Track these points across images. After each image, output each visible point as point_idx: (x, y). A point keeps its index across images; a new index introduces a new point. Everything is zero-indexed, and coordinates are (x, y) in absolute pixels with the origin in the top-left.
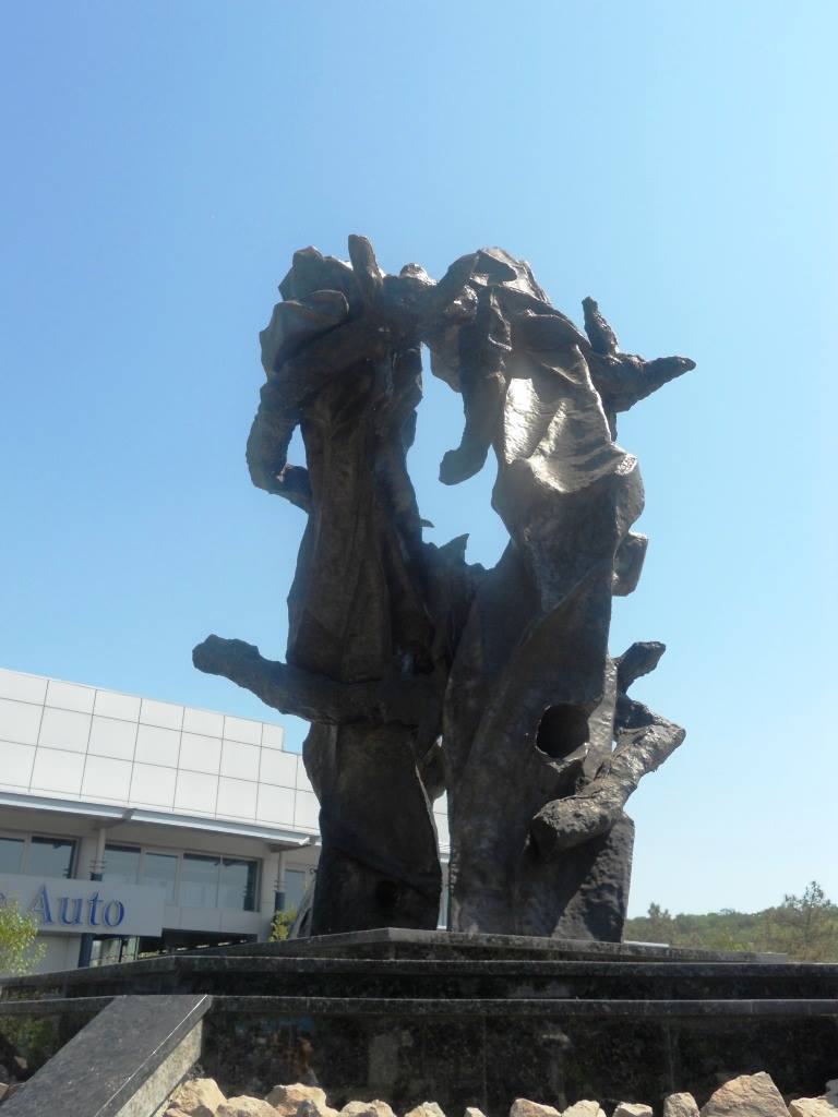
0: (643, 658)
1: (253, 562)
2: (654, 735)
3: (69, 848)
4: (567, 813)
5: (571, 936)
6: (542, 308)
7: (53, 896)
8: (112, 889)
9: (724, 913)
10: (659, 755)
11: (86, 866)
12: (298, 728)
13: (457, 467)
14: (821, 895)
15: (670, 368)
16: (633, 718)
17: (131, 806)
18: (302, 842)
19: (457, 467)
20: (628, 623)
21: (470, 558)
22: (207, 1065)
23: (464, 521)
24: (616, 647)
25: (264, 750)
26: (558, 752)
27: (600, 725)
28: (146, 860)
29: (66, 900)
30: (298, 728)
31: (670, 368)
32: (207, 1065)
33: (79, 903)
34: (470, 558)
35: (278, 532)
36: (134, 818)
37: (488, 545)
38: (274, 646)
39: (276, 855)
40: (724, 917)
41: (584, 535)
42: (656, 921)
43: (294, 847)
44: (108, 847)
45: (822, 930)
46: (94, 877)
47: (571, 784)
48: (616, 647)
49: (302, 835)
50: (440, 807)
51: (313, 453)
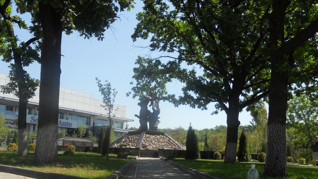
0: (159, 118)
4: (155, 126)
8: (70, 121)
9: (167, 129)
12: (139, 119)
16: (158, 121)
18: (99, 115)
19: (150, 106)
20: (159, 116)
23: (150, 109)
24: (158, 117)
28: (74, 117)
33: (65, 123)
35: (139, 108)
36: (75, 111)
37: (152, 111)
38: (139, 115)
39: (93, 117)
40: (167, 130)
41: (157, 112)
42: (159, 129)
43: (98, 116)
44: (69, 115)
45: (180, 133)
46: (67, 119)
47: (155, 125)
48: (158, 117)
50: (148, 124)
51: (74, 5)
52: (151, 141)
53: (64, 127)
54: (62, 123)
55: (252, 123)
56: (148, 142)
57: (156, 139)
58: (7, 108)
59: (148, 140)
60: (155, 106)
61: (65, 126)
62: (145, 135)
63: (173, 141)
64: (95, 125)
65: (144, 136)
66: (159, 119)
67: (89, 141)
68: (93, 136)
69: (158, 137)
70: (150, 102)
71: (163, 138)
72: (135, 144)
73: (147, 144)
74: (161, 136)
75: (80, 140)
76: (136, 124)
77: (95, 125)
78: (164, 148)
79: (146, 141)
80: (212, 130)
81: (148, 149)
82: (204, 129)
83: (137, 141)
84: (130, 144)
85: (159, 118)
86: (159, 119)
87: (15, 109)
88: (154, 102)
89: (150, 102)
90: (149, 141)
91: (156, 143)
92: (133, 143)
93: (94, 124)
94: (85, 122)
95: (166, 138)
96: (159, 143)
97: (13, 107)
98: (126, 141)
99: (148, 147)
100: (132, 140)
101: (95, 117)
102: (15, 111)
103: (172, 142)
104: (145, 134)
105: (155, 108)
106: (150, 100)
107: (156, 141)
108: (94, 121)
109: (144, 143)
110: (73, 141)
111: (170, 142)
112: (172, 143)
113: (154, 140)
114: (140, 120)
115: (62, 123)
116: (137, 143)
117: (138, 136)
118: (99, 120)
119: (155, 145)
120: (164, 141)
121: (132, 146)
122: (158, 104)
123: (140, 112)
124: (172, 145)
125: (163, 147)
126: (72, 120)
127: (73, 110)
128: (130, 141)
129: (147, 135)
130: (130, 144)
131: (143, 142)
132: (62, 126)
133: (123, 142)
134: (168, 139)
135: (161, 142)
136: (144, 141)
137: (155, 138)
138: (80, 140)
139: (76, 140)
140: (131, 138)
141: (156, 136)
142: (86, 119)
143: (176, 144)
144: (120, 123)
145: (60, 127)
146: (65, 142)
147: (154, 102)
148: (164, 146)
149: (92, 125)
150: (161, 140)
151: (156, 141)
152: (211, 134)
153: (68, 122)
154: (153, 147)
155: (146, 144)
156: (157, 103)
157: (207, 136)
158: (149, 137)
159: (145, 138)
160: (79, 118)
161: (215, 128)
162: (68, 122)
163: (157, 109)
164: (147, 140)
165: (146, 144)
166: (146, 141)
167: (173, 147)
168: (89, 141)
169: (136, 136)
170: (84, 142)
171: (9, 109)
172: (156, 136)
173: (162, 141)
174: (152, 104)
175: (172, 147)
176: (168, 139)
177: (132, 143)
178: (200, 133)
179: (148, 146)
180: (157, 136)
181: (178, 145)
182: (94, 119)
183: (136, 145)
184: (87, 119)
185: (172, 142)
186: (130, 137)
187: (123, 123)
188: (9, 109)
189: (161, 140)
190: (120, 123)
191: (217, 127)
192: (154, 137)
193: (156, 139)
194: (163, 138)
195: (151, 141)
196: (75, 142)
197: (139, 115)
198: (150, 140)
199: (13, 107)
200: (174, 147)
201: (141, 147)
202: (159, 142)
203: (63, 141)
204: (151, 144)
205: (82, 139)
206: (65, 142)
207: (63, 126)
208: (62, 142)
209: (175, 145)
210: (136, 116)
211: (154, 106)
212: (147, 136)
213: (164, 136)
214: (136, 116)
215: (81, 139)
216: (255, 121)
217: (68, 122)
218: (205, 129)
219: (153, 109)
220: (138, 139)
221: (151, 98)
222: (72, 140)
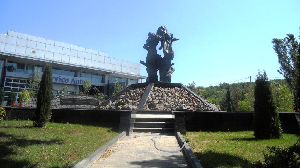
0: (173, 64)
1: (144, 55)
2: (173, 70)
3: (74, 72)
5: (167, 82)
6: (167, 35)
7: (75, 79)
8: (83, 79)
10: (173, 71)
11: (79, 75)
12: (146, 67)
13: (160, 49)
14: (194, 83)
15: (177, 40)
16: (172, 69)
17: (53, 60)
18: (113, 72)
19: (160, 49)
20: (172, 62)
21: (161, 56)
22: (154, 86)
23: (160, 53)
25: (99, 56)
26: (167, 71)
27: (170, 70)
28: (88, 75)
29: (128, 79)
30: (146, 67)
31: (177, 40)
32: (154, 86)
33: (79, 81)
34: (161, 56)
35: (145, 52)
36: (87, 68)
37: (163, 56)
38: (145, 62)
39: (108, 74)
41: (170, 56)
44: (82, 72)
46: (81, 77)
47: (168, 73)
49: (113, 71)
52: (162, 97)
53: (78, 84)
54: (75, 81)
55: (281, 71)
56: (157, 98)
57: (169, 94)
58: (18, 66)
59: (157, 94)
60: (167, 48)
61: (79, 83)
62: (153, 88)
63: (195, 96)
64: (110, 83)
65: (152, 89)
66: (173, 67)
67: (94, 98)
68: (101, 92)
69: (173, 90)
70: (160, 42)
71: (180, 92)
72: (138, 101)
73: (156, 101)
74: (176, 88)
75: (82, 98)
76: (143, 73)
77: (110, 83)
78: (182, 108)
79: (154, 96)
80: (216, 87)
81: (157, 109)
82: (210, 87)
83: (141, 97)
84: (130, 101)
85: (173, 64)
86: (173, 67)
87: (27, 67)
88: (165, 43)
89: (160, 42)
90: (159, 96)
91: (169, 98)
92: (135, 99)
93: (108, 81)
94: (100, 80)
95: (184, 91)
96: (175, 99)
97: (25, 65)
98: (125, 97)
99: (157, 106)
100: (134, 95)
101: (109, 74)
102: (27, 69)
103: (193, 96)
104: (153, 86)
105: (167, 51)
106: (159, 39)
107: (170, 97)
108: (108, 78)
109: (151, 100)
110: (74, 99)
111: (190, 97)
112: (193, 98)
113: (167, 94)
114: (147, 69)
115: (75, 81)
116: (140, 100)
117: (143, 90)
118: (114, 78)
119: (168, 102)
120: (182, 96)
121: (133, 104)
122: (170, 45)
123: (147, 58)
124: (194, 101)
125: (181, 105)
126: (86, 78)
127: (85, 68)
128: (131, 96)
129: (157, 88)
130: (130, 101)
131: (150, 97)
132: (75, 83)
133: (123, 99)
134: (187, 93)
135: (177, 97)
136: (152, 96)
137: (169, 92)
138: (82, 97)
139: (76, 98)
140: (134, 92)
141: (169, 89)
142: (101, 77)
143: (200, 100)
144: (135, 80)
145: (55, 83)
146: (63, 100)
147: (165, 43)
148: (182, 103)
149: (106, 83)
150: (177, 95)
151: (170, 97)
152: (216, 90)
153: (81, 80)
154: (166, 106)
155: (154, 101)
156: (170, 44)
157: (229, 90)
158: (159, 90)
159: (153, 92)
160: (95, 76)
161: (219, 85)
162: (81, 79)
163: (169, 51)
164: (156, 94)
165: (154, 101)
166: (154, 96)
167: (196, 104)
168: (94, 98)
169: (141, 89)
170: (87, 99)
171: (20, 67)
172: (169, 89)
173: (178, 96)
174: (162, 45)
175: (194, 105)
176: (187, 93)
177: (133, 99)
178: (206, 90)
179: (157, 104)
180: (171, 89)
181: (202, 102)
182: (108, 77)
183: (138, 103)
184: (102, 77)
185: (193, 96)
186: (132, 91)
187: (138, 80)
188: (20, 67)
189: (177, 95)
190: (135, 80)
191: (221, 84)
192: (166, 90)
193: (169, 94)
194: (180, 92)
195: (162, 97)
196: (76, 100)
197: (145, 62)
198: (160, 95)
199: (25, 65)
200: (198, 105)
201: (146, 105)
202: (175, 97)
203: (61, 99)
204: (162, 101)
205: (88, 96)
206: (63, 100)
207: (76, 84)
208: (59, 100)
209: (198, 101)
210: (142, 62)
211: (165, 48)
212: (156, 89)
213: (181, 88)
214: (142, 62)
215: (83, 97)
216: (283, 69)
217: (81, 79)
218: (211, 86)
219: (164, 52)
220: (143, 93)
221: (160, 37)
222: (72, 97)
